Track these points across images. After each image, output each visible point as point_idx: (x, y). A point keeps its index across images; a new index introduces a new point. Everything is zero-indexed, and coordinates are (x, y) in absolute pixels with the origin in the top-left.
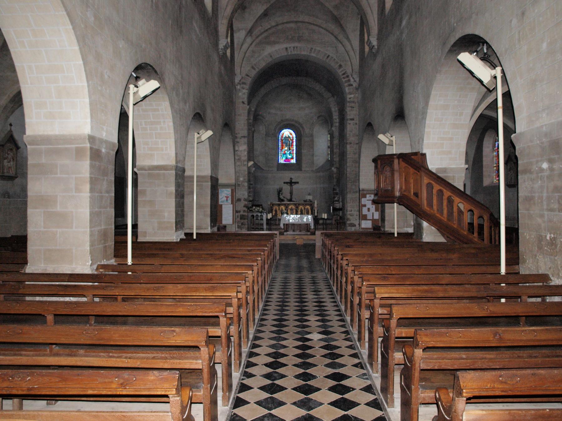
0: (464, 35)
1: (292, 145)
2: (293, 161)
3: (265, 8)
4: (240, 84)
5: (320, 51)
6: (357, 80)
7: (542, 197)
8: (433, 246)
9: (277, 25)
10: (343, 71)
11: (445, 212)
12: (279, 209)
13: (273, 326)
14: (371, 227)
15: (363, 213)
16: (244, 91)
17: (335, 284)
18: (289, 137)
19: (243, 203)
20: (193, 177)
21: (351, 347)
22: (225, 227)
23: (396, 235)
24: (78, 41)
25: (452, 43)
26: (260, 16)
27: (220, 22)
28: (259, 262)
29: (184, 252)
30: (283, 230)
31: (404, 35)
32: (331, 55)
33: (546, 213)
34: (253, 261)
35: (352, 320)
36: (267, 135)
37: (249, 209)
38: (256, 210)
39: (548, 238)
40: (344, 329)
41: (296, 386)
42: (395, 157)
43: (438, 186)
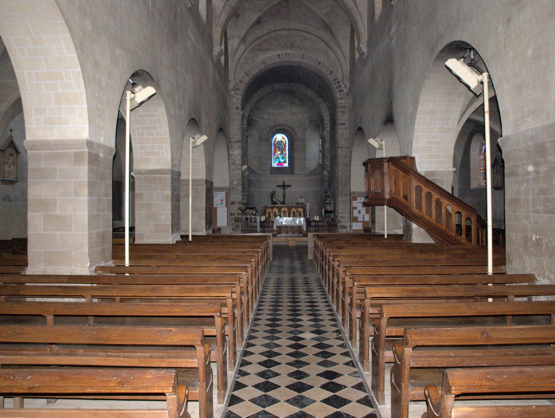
1: (285, 150)
2: (286, 165)
3: (258, 16)
5: (311, 57)
6: (348, 85)
8: (422, 248)
9: (270, 33)
11: (434, 214)
12: (272, 212)
13: (267, 325)
14: (361, 229)
15: (354, 216)
16: (238, 97)
17: (327, 285)
18: (282, 141)
19: (237, 206)
20: (188, 181)
21: (342, 346)
22: (219, 229)
23: (386, 237)
24: (76, 49)
25: (440, 49)
28: (253, 264)
29: (180, 254)
31: (393, 42)
32: (322, 61)
33: (532, 214)
34: (247, 263)
35: (343, 320)
36: (260, 139)
37: (243, 211)
38: (250, 212)
39: (534, 239)
40: (336, 329)
41: (289, 384)
42: (385, 160)
43: (426, 188)
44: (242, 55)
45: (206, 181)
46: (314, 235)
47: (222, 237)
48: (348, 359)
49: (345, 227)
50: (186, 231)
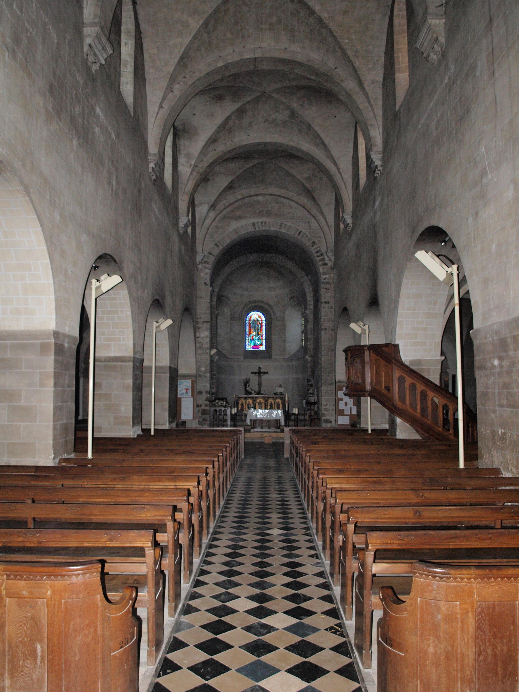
0: (429, 226)
1: (261, 330)
2: (263, 348)
3: (230, 181)
4: (202, 263)
5: (290, 227)
6: (333, 258)
7: (495, 393)
8: (404, 443)
9: (244, 198)
10: (317, 248)
11: (419, 407)
12: (246, 403)
13: (234, 522)
14: (348, 423)
17: (300, 483)
18: (258, 320)
19: (205, 396)
21: (309, 541)
22: (184, 423)
23: (370, 432)
24: (46, 241)
25: (420, 232)
26: (224, 189)
27: (180, 198)
30: (250, 427)
31: (377, 217)
32: (303, 231)
33: (497, 408)
34: (214, 457)
35: (312, 518)
36: (232, 318)
37: (211, 402)
38: (220, 404)
39: (500, 433)
40: (305, 526)
41: (253, 571)
42: (366, 348)
43: (410, 379)
44: (211, 224)
45: (170, 368)
46: (290, 430)
47: (188, 430)
48: (313, 552)
49: (328, 421)
50: (147, 425)
